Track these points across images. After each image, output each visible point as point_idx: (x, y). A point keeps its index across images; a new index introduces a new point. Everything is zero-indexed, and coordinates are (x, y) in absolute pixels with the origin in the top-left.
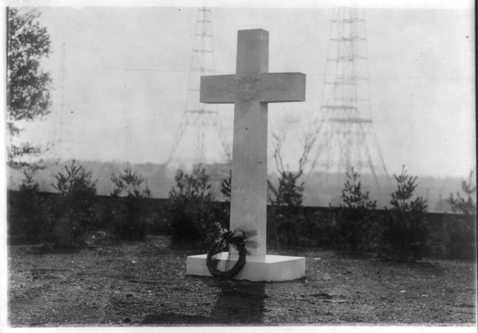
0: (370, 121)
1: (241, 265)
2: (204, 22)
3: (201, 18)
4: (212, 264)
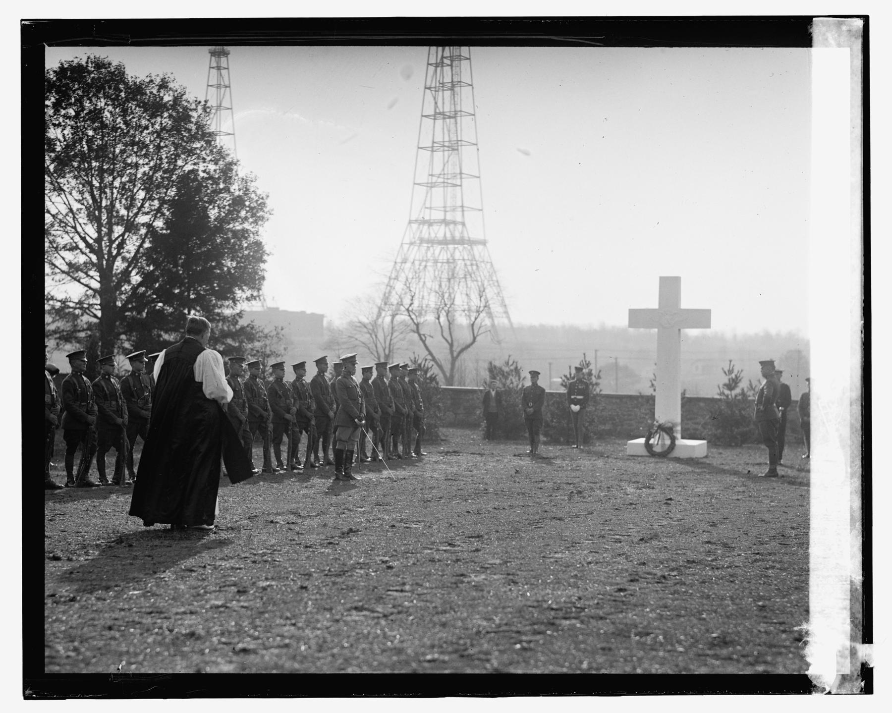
0: (484, 243)
1: (673, 446)
2: (219, 86)
3: (214, 81)
4: (648, 446)
